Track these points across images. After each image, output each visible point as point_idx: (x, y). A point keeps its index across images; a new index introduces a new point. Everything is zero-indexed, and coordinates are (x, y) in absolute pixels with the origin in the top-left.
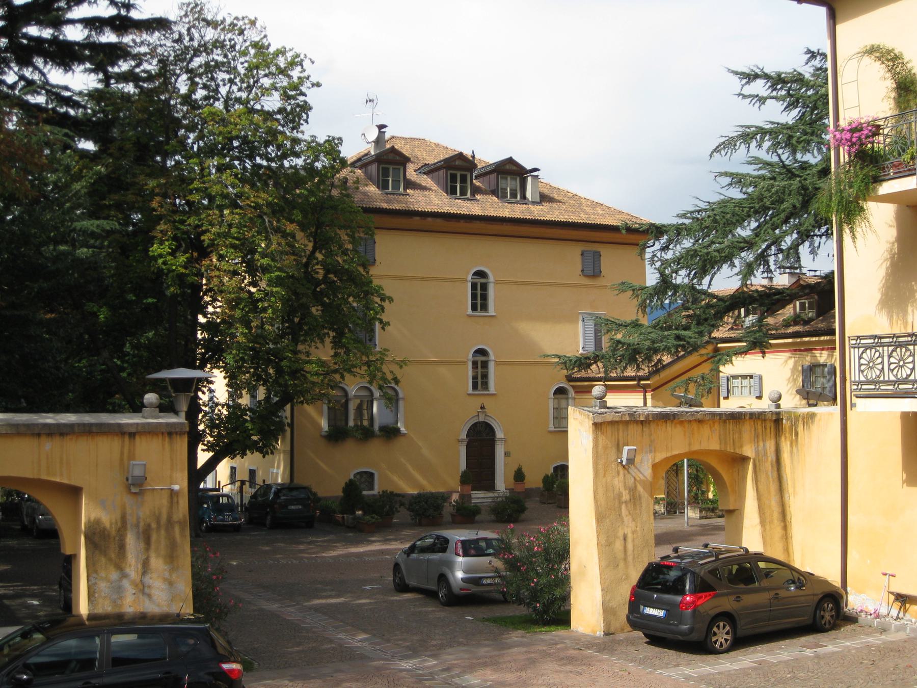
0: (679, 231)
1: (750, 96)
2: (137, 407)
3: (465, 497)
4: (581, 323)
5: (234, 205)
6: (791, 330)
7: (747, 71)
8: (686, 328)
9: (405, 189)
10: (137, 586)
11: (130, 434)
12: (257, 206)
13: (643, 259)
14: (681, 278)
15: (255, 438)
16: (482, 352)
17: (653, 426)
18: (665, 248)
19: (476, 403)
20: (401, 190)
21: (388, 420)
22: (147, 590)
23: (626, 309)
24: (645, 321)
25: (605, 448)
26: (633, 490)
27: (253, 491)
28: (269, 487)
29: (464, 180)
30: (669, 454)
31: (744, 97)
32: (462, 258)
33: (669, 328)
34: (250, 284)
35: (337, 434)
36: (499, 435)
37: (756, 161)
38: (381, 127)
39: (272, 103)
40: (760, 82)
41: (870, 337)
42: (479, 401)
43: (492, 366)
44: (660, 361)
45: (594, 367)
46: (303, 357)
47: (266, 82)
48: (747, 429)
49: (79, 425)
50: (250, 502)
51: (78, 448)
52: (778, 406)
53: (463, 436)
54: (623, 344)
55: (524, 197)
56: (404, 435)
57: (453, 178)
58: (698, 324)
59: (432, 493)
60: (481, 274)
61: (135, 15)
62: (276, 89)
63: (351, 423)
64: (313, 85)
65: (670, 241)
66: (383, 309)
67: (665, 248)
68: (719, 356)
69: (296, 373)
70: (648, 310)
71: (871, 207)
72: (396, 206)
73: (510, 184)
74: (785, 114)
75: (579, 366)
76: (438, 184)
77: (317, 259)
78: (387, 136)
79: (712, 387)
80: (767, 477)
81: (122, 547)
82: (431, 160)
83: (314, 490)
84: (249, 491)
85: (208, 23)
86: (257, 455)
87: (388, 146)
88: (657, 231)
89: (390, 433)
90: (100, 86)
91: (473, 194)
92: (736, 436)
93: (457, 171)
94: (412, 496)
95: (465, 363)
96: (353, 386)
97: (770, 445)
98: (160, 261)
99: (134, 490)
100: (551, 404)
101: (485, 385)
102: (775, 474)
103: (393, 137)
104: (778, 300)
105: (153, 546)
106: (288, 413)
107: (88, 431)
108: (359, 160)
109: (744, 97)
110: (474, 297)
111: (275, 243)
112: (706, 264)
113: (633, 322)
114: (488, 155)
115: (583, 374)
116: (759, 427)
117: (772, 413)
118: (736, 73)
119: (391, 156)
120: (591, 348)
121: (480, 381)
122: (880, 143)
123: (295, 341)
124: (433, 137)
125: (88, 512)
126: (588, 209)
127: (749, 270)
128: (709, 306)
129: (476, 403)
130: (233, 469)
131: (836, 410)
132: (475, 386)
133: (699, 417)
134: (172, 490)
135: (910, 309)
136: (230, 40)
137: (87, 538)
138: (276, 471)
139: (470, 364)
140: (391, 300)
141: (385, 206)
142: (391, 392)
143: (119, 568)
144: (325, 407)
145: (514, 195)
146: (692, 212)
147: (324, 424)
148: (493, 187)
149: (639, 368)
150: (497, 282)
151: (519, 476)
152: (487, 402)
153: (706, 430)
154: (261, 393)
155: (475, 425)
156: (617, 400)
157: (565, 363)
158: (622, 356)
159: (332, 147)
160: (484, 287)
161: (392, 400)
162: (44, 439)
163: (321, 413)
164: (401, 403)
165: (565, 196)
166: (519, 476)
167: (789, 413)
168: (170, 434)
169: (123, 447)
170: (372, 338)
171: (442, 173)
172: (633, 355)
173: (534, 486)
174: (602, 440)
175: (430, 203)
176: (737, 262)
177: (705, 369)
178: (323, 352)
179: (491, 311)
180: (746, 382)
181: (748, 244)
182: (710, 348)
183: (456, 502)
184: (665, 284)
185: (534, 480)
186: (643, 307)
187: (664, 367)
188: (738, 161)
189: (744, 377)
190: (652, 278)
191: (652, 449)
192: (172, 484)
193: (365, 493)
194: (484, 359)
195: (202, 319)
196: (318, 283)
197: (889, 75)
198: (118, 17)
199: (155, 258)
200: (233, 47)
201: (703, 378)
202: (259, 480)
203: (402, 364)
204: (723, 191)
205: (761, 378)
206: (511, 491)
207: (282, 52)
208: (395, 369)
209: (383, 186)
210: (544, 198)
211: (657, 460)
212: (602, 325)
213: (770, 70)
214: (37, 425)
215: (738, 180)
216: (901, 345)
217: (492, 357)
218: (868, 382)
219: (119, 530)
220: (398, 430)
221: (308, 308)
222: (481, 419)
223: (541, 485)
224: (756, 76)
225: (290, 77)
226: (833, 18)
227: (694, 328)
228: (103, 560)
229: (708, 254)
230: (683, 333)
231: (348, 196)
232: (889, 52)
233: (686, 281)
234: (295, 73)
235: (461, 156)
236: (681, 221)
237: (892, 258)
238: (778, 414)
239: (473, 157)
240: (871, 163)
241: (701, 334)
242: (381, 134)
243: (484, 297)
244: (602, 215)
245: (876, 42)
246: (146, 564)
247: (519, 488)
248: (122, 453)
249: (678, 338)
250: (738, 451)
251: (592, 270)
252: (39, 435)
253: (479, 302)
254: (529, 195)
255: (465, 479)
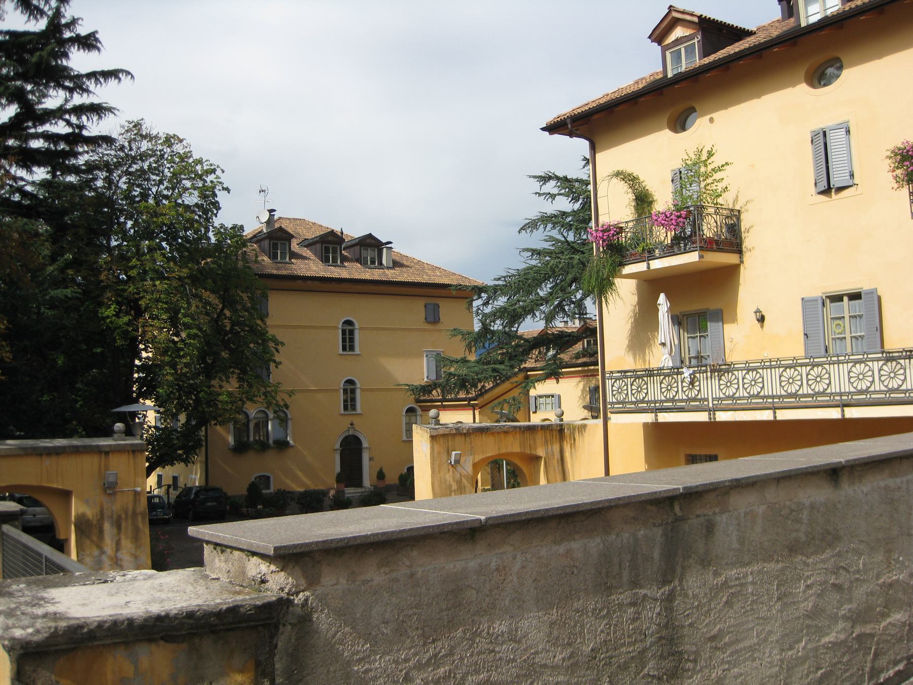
0: (495, 291)
1: (544, 194)
2: (108, 432)
3: (340, 493)
4: (425, 359)
5: (162, 278)
6: (580, 361)
7: (543, 175)
8: (501, 363)
9: (290, 259)
10: (112, 559)
11: (105, 452)
12: (180, 279)
13: (471, 312)
14: (497, 326)
15: (180, 452)
16: (350, 382)
17: (473, 437)
18: (486, 304)
19: (347, 421)
20: (287, 259)
21: (280, 435)
22: (119, 562)
23: (457, 349)
24: (472, 358)
25: (439, 453)
26: (459, 482)
27: (178, 493)
28: (190, 489)
29: (335, 252)
30: (484, 456)
31: (540, 195)
32: (335, 311)
33: (488, 363)
34: (174, 334)
35: (241, 447)
36: (365, 444)
37: (551, 239)
38: (271, 211)
39: (192, 199)
40: (552, 183)
41: (619, 372)
42: (349, 420)
43: (358, 392)
44: (483, 387)
45: (434, 392)
46: (218, 389)
47: (188, 184)
48: (539, 436)
49: (82, 446)
50: (176, 501)
51: (69, 464)
52: (562, 420)
53: (338, 446)
54: (455, 375)
55: (381, 263)
56: (293, 446)
57: (327, 250)
58: (510, 359)
59: (315, 490)
60: (349, 323)
61: (85, 133)
62: (195, 189)
63: (251, 439)
64: (224, 189)
65: (489, 298)
66: (277, 351)
67: (486, 304)
68: (528, 381)
69: (212, 402)
70: (473, 349)
71: (618, 281)
72: (284, 272)
73: (369, 254)
74: (571, 204)
75: (424, 392)
76: (315, 254)
77: (225, 315)
78: (276, 217)
79: (524, 404)
80: (555, 470)
81: (101, 532)
82: (310, 235)
83: (224, 490)
84: (174, 494)
85: (144, 137)
86: (182, 464)
87: (277, 226)
88: (479, 290)
89: (282, 445)
90: (48, 177)
91: (342, 262)
92: (532, 442)
93: (330, 244)
94: (300, 493)
95: (337, 390)
96: (252, 410)
97: (556, 448)
98: (108, 321)
99: (109, 492)
100: (404, 420)
101: (354, 407)
102: (560, 467)
103: (280, 218)
104: (568, 341)
105: (123, 531)
106: (203, 433)
107: (77, 451)
108: (255, 236)
109: (540, 195)
110: (344, 340)
111: (194, 306)
112: (514, 316)
113: (462, 359)
114: (354, 231)
115: (426, 397)
116: (548, 435)
117: (557, 425)
118: (535, 177)
119: (279, 234)
120: (433, 377)
121: (350, 403)
122: (623, 239)
123: (209, 377)
124: (310, 218)
125: (76, 508)
126: (429, 272)
127: (549, 318)
128: (517, 346)
129: (347, 421)
130: (160, 477)
131: (600, 422)
132: (346, 408)
133: (505, 429)
134: (135, 492)
135: (647, 351)
136: (160, 151)
137: (75, 526)
138: (194, 476)
139: (342, 391)
140: (283, 344)
141: (275, 272)
142: (282, 415)
143: (99, 547)
144: (232, 427)
145: (373, 262)
146: (504, 277)
147: (231, 440)
148: (357, 256)
149: (468, 393)
150: (361, 329)
151: (381, 475)
152: (356, 420)
153: (510, 438)
154: (182, 418)
155: (346, 437)
156: (449, 418)
157: (413, 390)
158: (455, 384)
159: (238, 229)
160: (352, 332)
161: (283, 421)
162: (44, 458)
163: (228, 432)
164: (290, 423)
165: (412, 262)
166: (381, 475)
167: (569, 425)
168: (134, 452)
169: (100, 462)
170: (269, 374)
171: (318, 246)
172: (463, 383)
173: (392, 483)
174: (436, 447)
175: (310, 269)
176: (537, 314)
177: (516, 393)
178: (232, 385)
179: (357, 350)
180: (549, 400)
181: (545, 300)
182: (521, 376)
183: (333, 496)
184: (485, 329)
185: (392, 478)
186: (469, 347)
187: (487, 391)
188: (539, 239)
189: (547, 396)
190: (477, 327)
191: (472, 452)
192: (135, 486)
193: (264, 491)
194: (352, 387)
195: (137, 362)
196: (226, 333)
197: (630, 190)
198: (72, 134)
199: (104, 319)
200: (162, 156)
201: (514, 399)
202: (181, 483)
203: (291, 393)
204: (529, 262)
205: (559, 397)
206: (375, 487)
207: (200, 162)
208: (286, 397)
209: (273, 257)
210: (396, 264)
211: (476, 461)
212: (441, 361)
213: (561, 175)
214: (41, 447)
215: (535, 252)
216: (639, 377)
217: (358, 385)
218: (618, 403)
219: (99, 520)
220: (288, 443)
221: (219, 354)
222: (351, 433)
223: (397, 482)
224: (550, 178)
225: (205, 181)
226: (593, 149)
227: (507, 363)
228: (88, 542)
229: (515, 309)
230: (498, 366)
231: (249, 268)
232: (629, 175)
233: (501, 328)
234: (211, 178)
235: (332, 233)
236: (497, 283)
237: (635, 316)
238: (561, 425)
239: (342, 233)
240: (618, 251)
241: (512, 367)
242: (272, 216)
243: (352, 340)
244: (440, 276)
245: (620, 169)
246: (118, 545)
247: (381, 484)
248: (100, 466)
249: (494, 370)
250: (533, 453)
251: (433, 318)
252: (41, 455)
253: (348, 344)
254: (384, 262)
255: (339, 479)
